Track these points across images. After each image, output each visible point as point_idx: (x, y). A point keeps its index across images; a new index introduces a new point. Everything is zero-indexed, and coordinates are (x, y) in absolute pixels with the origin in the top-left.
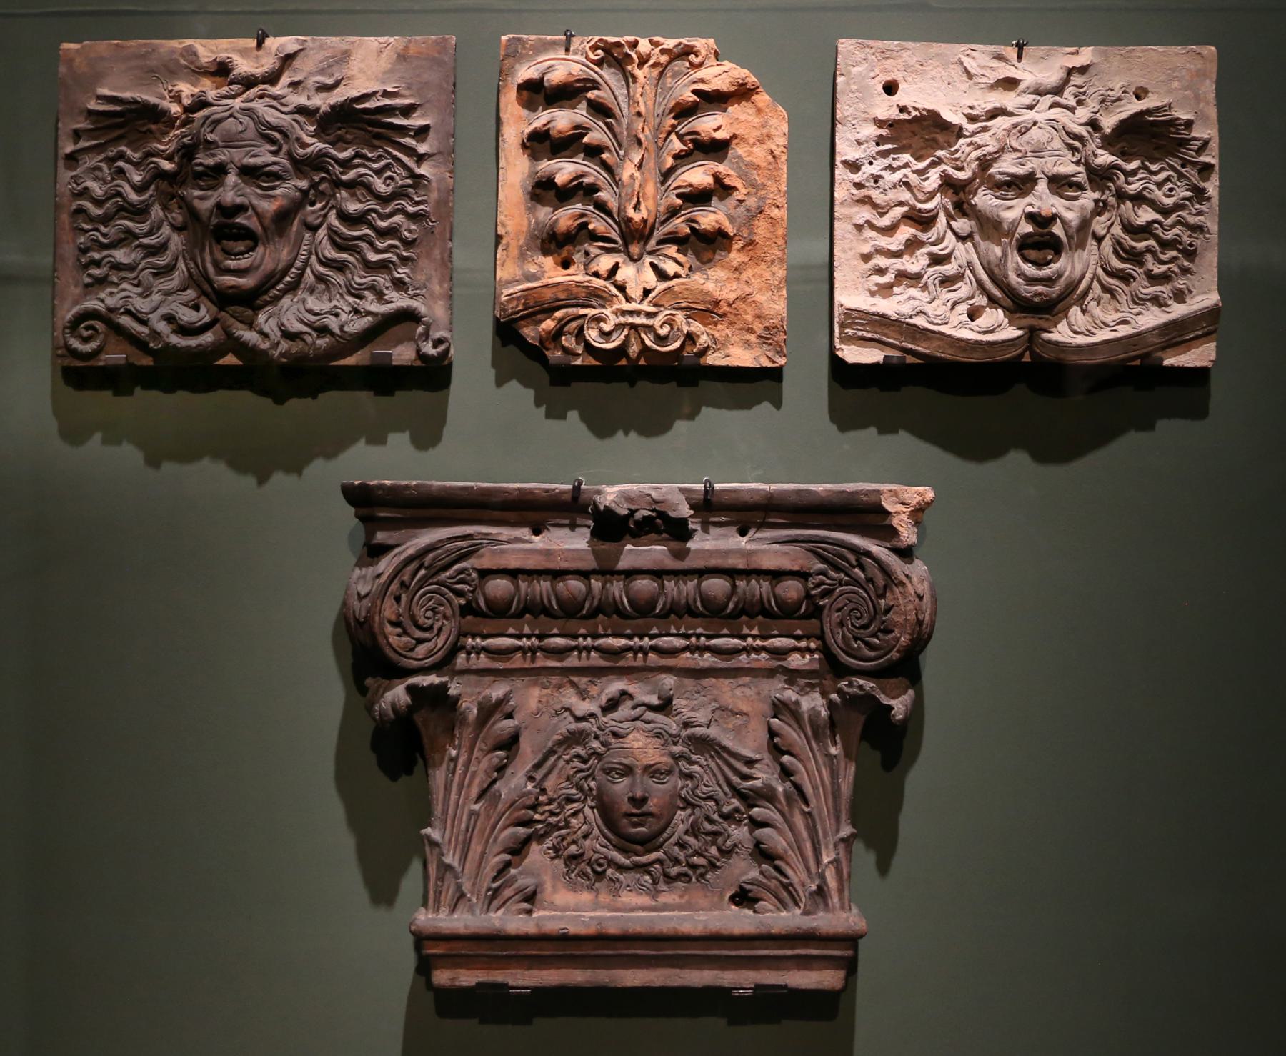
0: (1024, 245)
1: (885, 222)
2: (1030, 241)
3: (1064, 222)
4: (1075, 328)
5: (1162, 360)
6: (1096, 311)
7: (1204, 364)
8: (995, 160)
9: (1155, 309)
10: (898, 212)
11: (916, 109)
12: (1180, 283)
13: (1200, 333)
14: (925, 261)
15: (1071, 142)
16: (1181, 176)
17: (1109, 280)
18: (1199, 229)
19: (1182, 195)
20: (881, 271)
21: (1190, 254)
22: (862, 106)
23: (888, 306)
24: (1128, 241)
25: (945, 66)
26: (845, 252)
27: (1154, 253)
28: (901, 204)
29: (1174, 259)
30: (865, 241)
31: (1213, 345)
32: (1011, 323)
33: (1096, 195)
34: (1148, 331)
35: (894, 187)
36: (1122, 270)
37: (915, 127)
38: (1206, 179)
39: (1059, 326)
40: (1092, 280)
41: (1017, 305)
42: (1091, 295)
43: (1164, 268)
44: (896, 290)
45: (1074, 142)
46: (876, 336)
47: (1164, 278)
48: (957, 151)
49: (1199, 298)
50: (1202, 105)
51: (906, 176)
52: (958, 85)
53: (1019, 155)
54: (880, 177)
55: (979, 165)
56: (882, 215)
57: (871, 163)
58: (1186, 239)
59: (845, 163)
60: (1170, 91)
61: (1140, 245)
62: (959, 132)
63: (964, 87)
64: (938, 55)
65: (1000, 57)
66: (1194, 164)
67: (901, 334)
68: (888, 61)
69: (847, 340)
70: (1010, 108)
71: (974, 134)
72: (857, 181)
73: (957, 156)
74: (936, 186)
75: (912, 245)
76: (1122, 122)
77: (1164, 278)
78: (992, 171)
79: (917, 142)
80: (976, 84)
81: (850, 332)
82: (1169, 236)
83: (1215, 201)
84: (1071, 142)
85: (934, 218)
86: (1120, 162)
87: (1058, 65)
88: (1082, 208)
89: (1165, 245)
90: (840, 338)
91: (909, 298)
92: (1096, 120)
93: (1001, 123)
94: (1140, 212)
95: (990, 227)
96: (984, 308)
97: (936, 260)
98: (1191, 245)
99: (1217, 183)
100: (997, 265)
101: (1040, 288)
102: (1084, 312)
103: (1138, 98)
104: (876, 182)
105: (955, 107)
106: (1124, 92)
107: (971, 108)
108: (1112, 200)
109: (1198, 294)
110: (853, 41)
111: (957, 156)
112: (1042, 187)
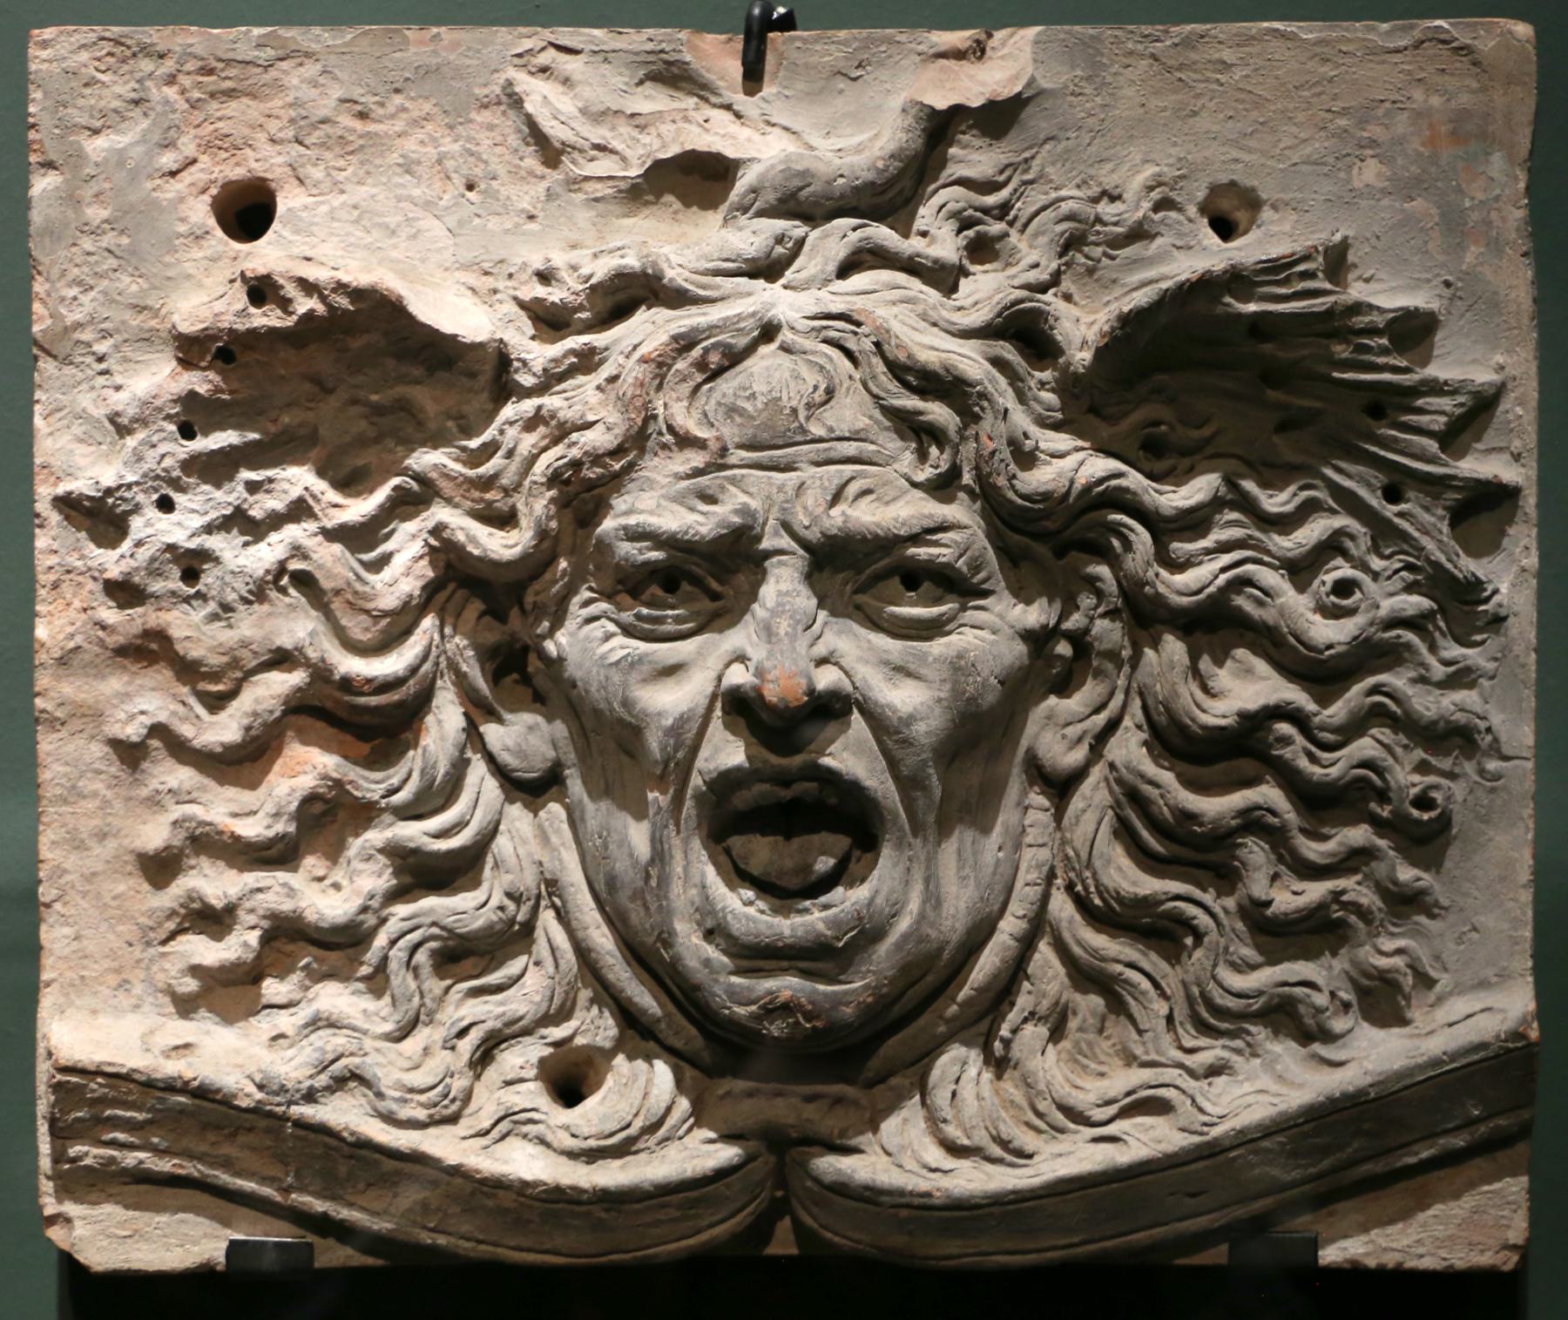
0: (729, 817)
1: (225, 729)
2: (743, 799)
3: (879, 722)
4: (952, 1131)
5: (1314, 1245)
6: (1049, 1066)
7: (1485, 1259)
8: (616, 481)
9: (1284, 1050)
10: (280, 684)
11: (309, 287)
12: (1385, 951)
13: (1459, 1141)
14: (374, 879)
15: (911, 402)
16: (1384, 534)
17: (1099, 941)
18: (1453, 739)
19: (1387, 606)
20: (211, 919)
21: (1426, 836)
22: (129, 285)
23: (232, 1056)
24: (1170, 788)
25: (455, 117)
26: (78, 845)
27: (1276, 837)
28: (282, 659)
29: (1354, 860)
30: (154, 802)
31: (1516, 1187)
32: (699, 1115)
33: (1035, 615)
34: (1246, 1139)
35: (259, 593)
36: (1146, 903)
37: (321, 360)
38: (1486, 546)
39: (890, 1126)
40: (1027, 944)
41: (712, 1049)
42: (1023, 1002)
43: (1315, 891)
44: (273, 989)
45: (925, 400)
46: (191, 1169)
47: (1317, 931)
48: (490, 449)
49: (1458, 1006)
50: (1472, 254)
51: (298, 551)
52: (505, 189)
53: (697, 459)
54: (204, 555)
55: (562, 504)
56: (216, 703)
57: (166, 505)
58: (1405, 778)
59: (68, 505)
60: (1349, 200)
61: (1216, 807)
62: (494, 374)
63: (527, 196)
64: (426, 72)
65: (673, 76)
66: (1434, 485)
67: (282, 1159)
68: (233, 107)
69: (83, 1183)
70: (674, 275)
71: (550, 380)
72: (114, 573)
73: (487, 469)
74: (410, 586)
75: (326, 821)
76: (1130, 322)
77: (1317, 931)
78: (608, 524)
79: (334, 418)
80: (575, 183)
81: (88, 1153)
82: (1335, 767)
83: (1523, 629)
84: (911, 402)
85: (421, 703)
86: (1134, 480)
87: (897, 102)
88: (959, 666)
89: (1323, 804)
90: (56, 1177)
91: (317, 1023)
92: (1039, 315)
93: (649, 329)
94: (1223, 677)
95: (610, 748)
96: (610, 1054)
97: (422, 874)
98: (1423, 802)
99: (1532, 561)
100: (638, 895)
101: (786, 985)
102: (999, 1065)
103: (1225, 228)
104: (191, 576)
105: (485, 275)
106: (1163, 204)
107: (545, 277)
108: (1108, 632)
109: (1459, 990)
110: (87, 34)
111: (487, 469)
112: (784, 586)
